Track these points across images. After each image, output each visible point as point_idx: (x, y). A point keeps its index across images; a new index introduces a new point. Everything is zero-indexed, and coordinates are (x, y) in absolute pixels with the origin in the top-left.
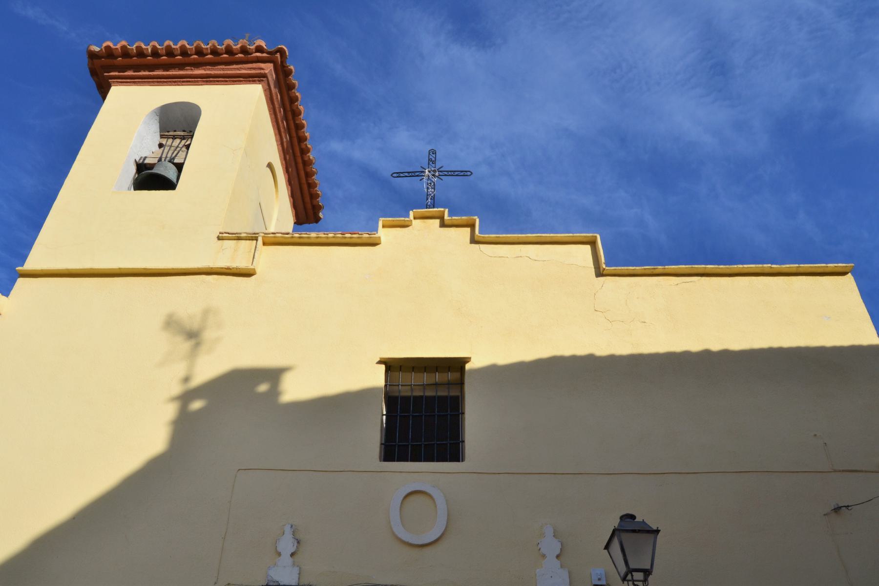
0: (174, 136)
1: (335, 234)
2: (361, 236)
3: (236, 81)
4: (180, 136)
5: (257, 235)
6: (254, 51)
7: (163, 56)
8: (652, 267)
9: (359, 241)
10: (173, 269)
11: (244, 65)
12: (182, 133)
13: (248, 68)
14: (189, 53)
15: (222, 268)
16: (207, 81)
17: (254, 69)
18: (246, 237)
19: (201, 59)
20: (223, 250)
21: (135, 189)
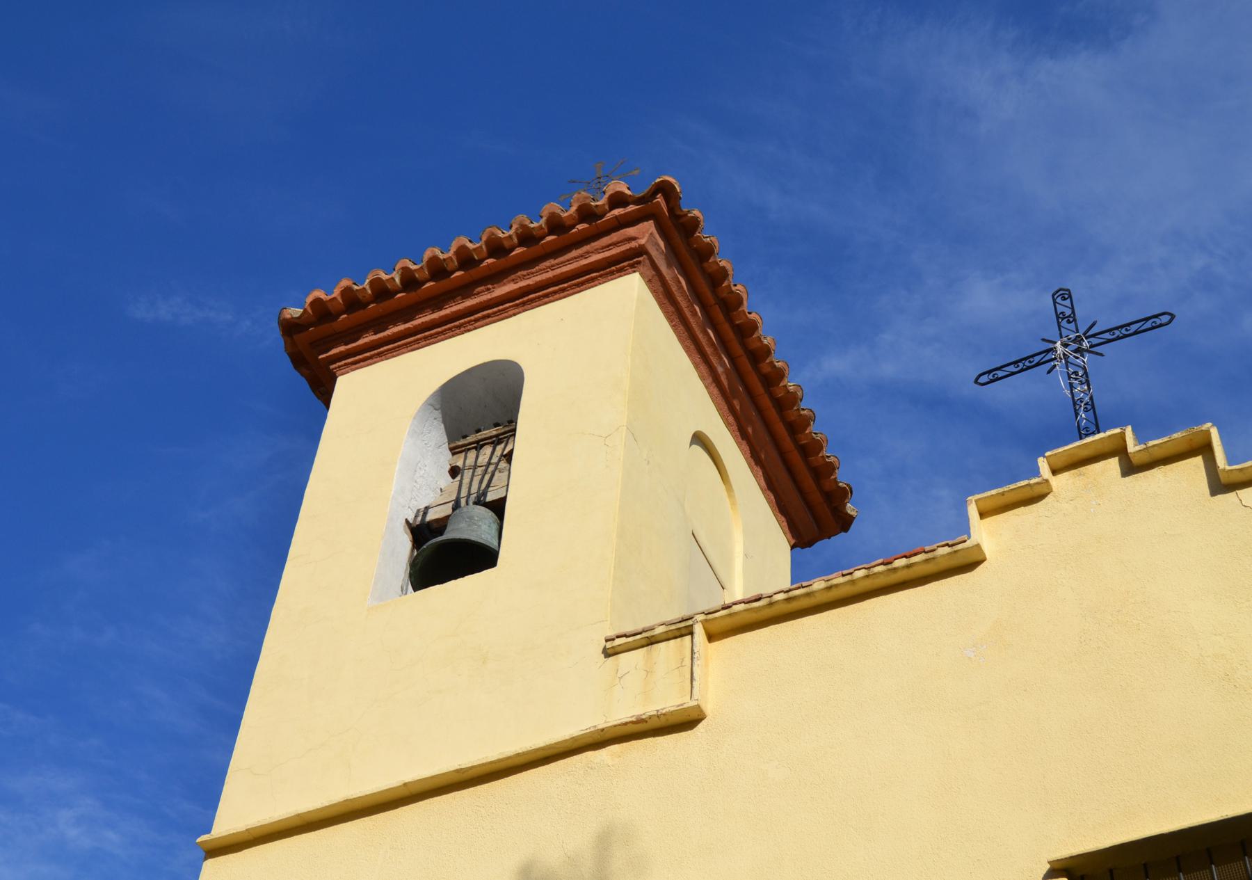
0: (477, 442)
2: (930, 555)
3: (583, 283)
4: (491, 437)
5: (690, 622)
6: (607, 207)
11: (593, 244)
12: (493, 432)
13: (603, 248)
14: (476, 257)
15: (626, 724)
16: (524, 304)
17: (616, 244)
21: (416, 589)
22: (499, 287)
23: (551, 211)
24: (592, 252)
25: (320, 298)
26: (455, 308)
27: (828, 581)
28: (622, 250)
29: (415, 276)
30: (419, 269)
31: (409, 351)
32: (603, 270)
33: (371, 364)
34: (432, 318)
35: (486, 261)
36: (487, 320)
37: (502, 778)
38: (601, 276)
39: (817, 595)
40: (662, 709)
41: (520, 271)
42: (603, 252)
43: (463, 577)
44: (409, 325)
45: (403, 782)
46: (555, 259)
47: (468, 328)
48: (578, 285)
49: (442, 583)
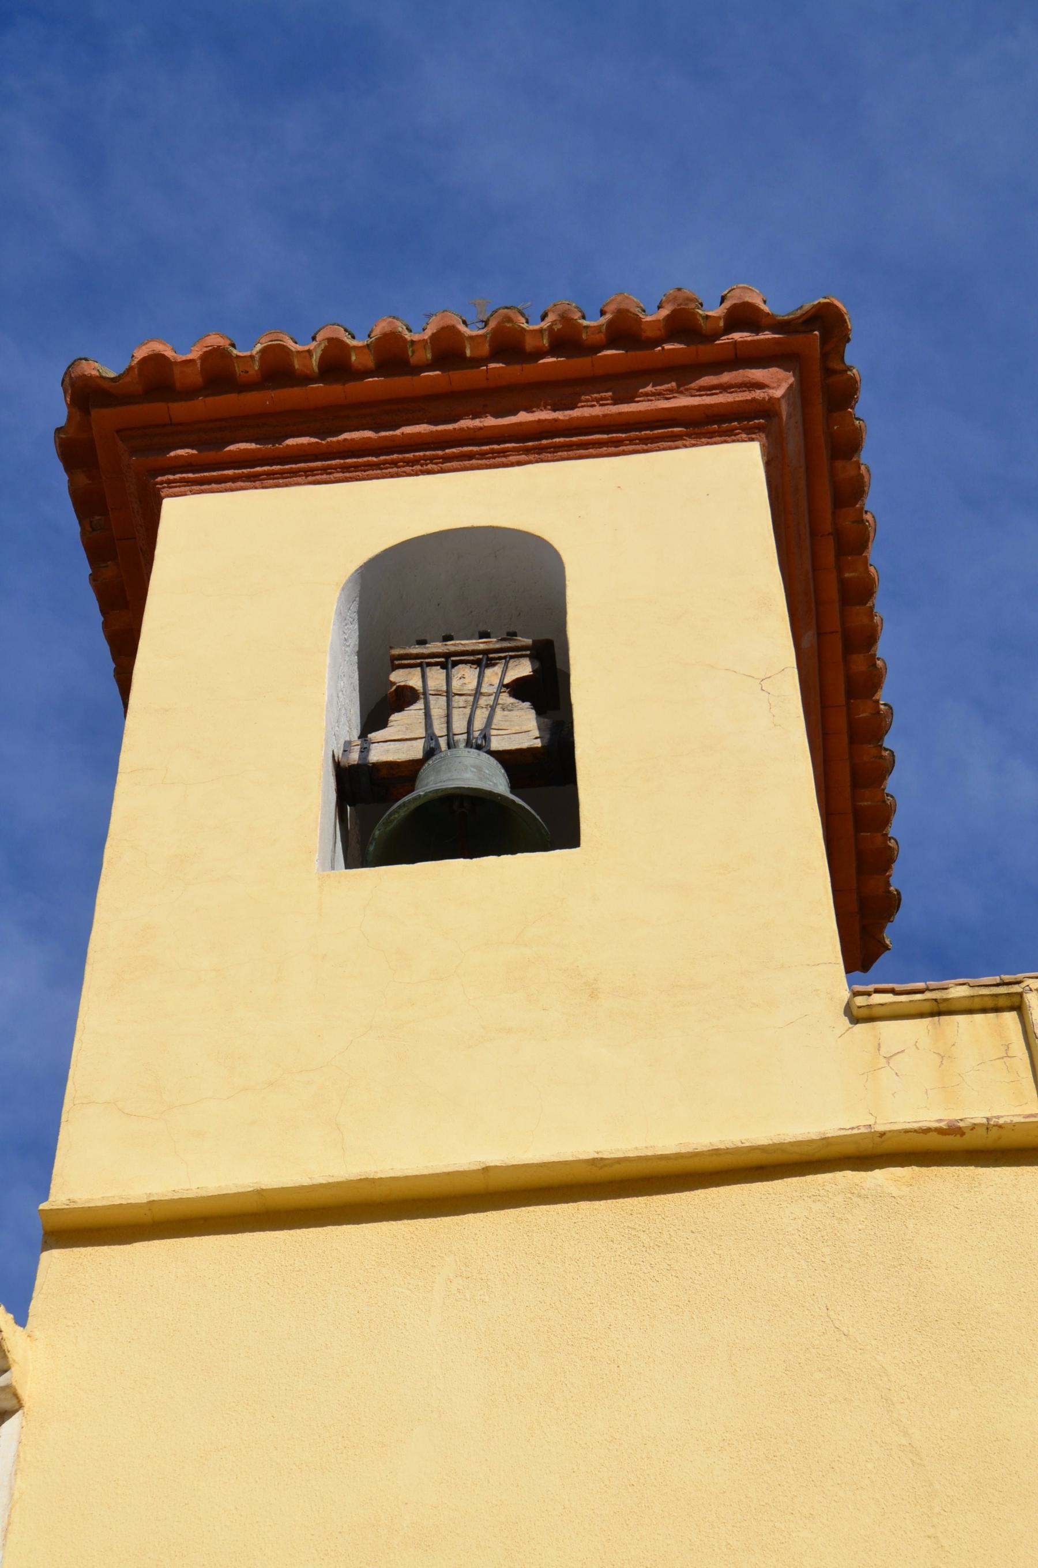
0: (447, 655)
4: (473, 653)
5: (1016, 989)
7: (544, 355)
10: (716, 1152)
12: (481, 645)
14: (468, 353)
15: (927, 1131)
17: (725, 388)
20: (888, 1059)
21: (348, 866)
23: (623, 306)
25: (163, 356)
28: (737, 399)
30: (363, 347)
33: (232, 490)
37: (381, 1221)
40: (998, 1117)
43: (499, 855)
44: (559, 415)
45: (483, 1166)
48: (644, 440)
49: (471, 858)
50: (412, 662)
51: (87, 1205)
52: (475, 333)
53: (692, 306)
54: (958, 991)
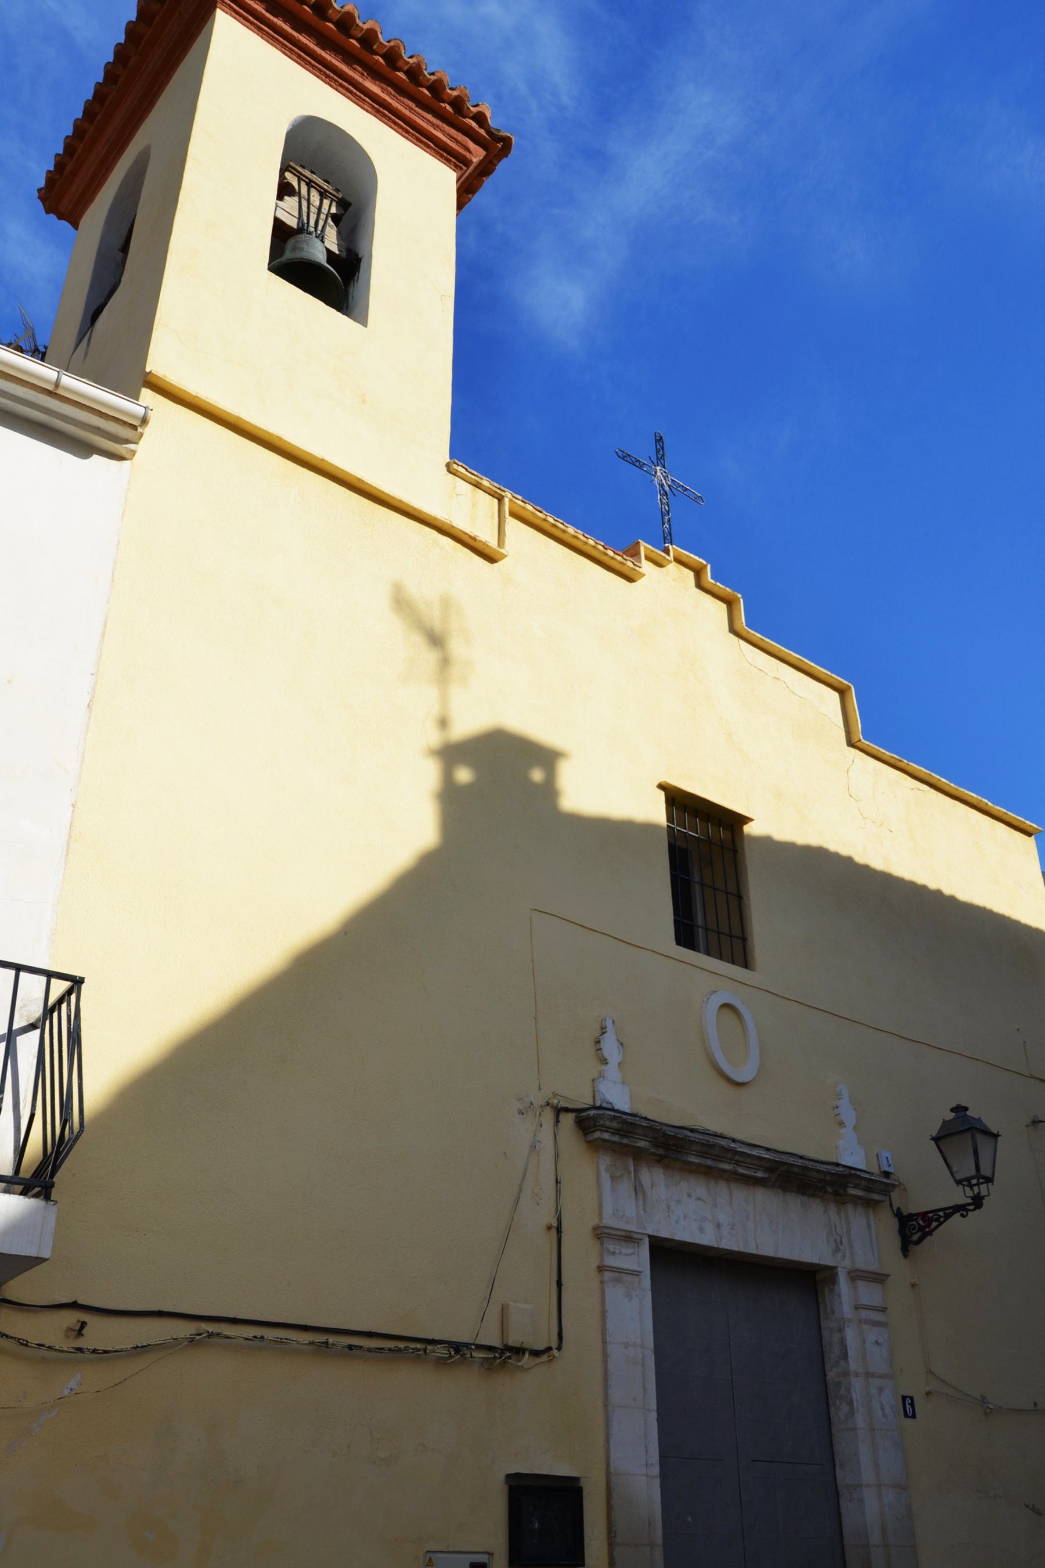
1: (596, 543)
2: (624, 561)
3: (421, 142)
6: (471, 115)
8: (899, 758)
9: (617, 566)
10: (400, 501)
11: (444, 125)
13: (448, 135)
14: (375, 47)
15: (466, 534)
16: (378, 111)
17: (457, 142)
18: (489, 488)
19: (387, 70)
22: (370, 81)
24: (441, 130)
26: (334, 61)
27: (576, 532)
29: (328, 10)
31: (281, 51)
32: (439, 148)
34: (316, 49)
35: (378, 57)
36: (348, 94)
38: (434, 150)
39: (625, 566)
41: (392, 88)
42: (447, 137)
44: (268, 15)
45: (322, 458)
46: (416, 106)
47: (332, 84)
48: (418, 139)
49: (327, 305)
50: (296, 173)
51: (171, 382)
52: (383, 42)
53: (466, 99)
54: (486, 482)
